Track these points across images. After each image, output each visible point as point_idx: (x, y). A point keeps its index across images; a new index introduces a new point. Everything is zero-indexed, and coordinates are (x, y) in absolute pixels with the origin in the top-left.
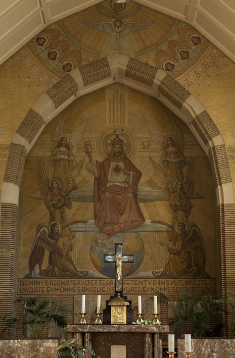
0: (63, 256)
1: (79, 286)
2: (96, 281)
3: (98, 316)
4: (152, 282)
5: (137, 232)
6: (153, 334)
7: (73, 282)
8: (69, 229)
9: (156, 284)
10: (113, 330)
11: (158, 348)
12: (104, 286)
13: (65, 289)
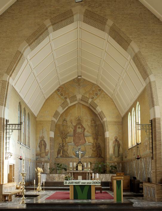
6: (88, 173)
10: (78, 172)
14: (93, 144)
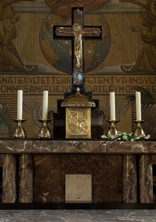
0: (5, 45)
1: (26, 84)
2: (48, 78)
3: (45, 124)
4: (121, 80)
5: (101, 14)
6: (137, 157)
7: (17, 79)
8: (12, 9)
9: (125, 82)
10: (68, 149)
11: (146, 179)
12: (58, 85)
13: (8, 89)
14: (147, 7)
